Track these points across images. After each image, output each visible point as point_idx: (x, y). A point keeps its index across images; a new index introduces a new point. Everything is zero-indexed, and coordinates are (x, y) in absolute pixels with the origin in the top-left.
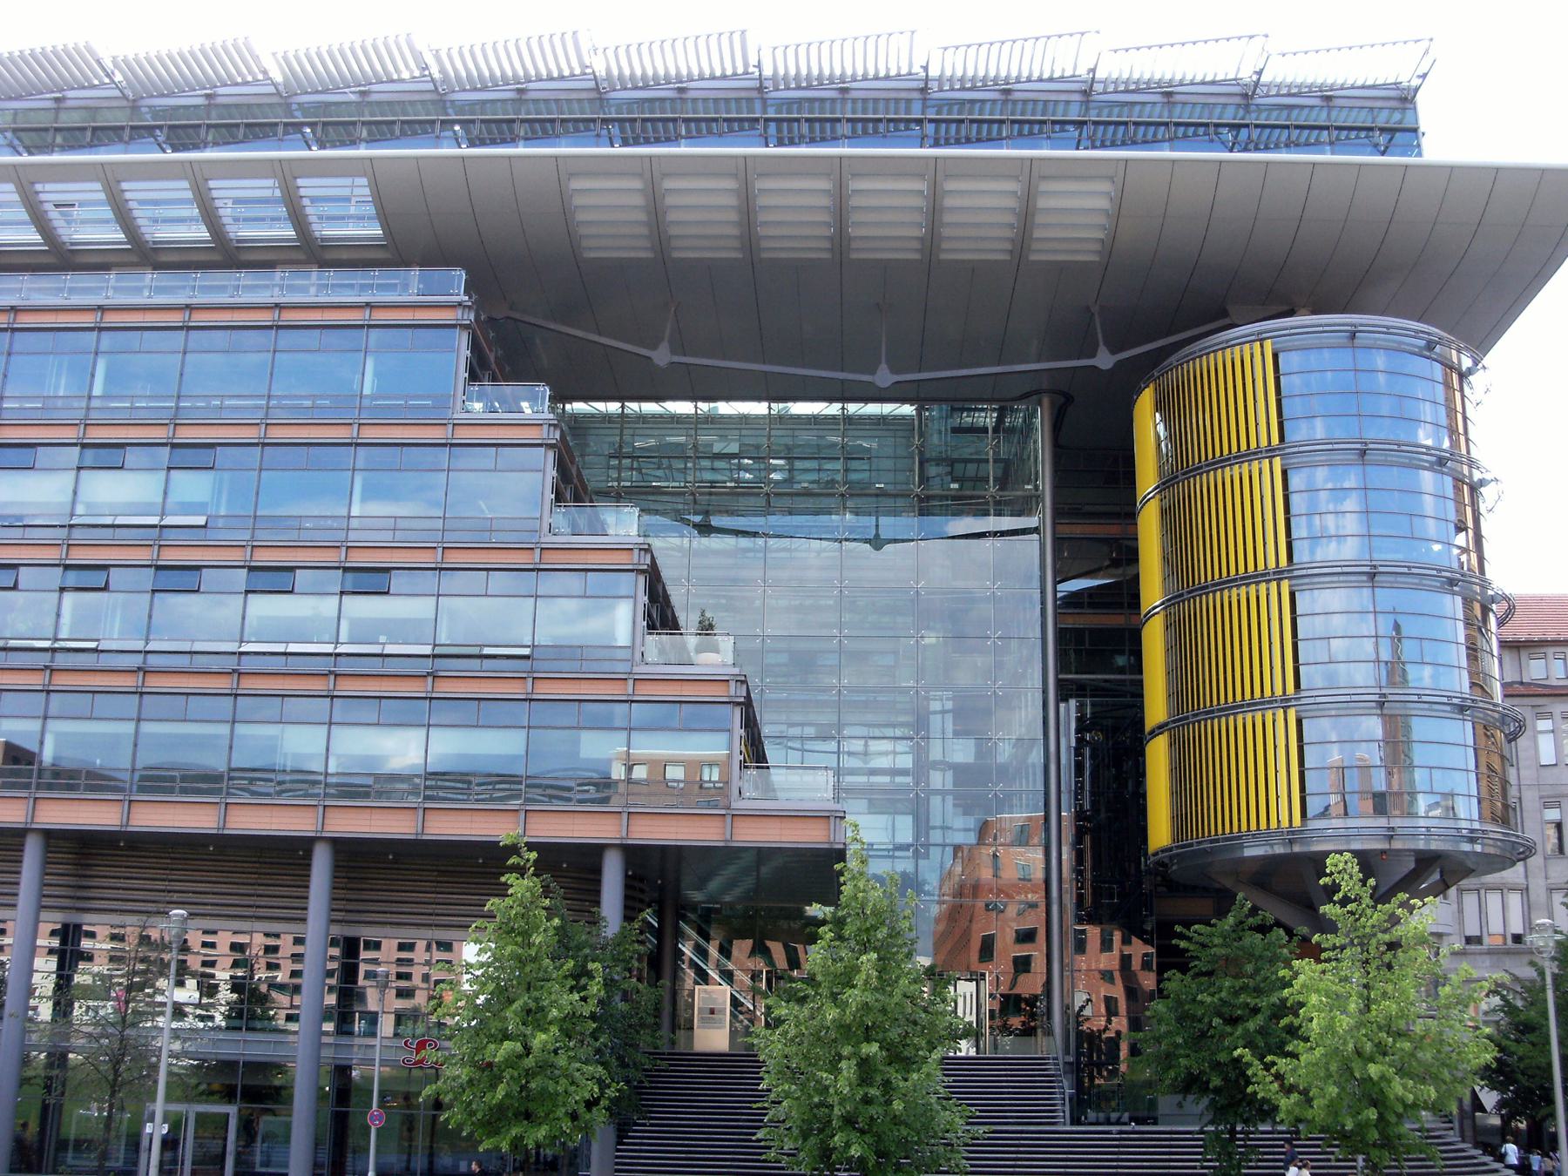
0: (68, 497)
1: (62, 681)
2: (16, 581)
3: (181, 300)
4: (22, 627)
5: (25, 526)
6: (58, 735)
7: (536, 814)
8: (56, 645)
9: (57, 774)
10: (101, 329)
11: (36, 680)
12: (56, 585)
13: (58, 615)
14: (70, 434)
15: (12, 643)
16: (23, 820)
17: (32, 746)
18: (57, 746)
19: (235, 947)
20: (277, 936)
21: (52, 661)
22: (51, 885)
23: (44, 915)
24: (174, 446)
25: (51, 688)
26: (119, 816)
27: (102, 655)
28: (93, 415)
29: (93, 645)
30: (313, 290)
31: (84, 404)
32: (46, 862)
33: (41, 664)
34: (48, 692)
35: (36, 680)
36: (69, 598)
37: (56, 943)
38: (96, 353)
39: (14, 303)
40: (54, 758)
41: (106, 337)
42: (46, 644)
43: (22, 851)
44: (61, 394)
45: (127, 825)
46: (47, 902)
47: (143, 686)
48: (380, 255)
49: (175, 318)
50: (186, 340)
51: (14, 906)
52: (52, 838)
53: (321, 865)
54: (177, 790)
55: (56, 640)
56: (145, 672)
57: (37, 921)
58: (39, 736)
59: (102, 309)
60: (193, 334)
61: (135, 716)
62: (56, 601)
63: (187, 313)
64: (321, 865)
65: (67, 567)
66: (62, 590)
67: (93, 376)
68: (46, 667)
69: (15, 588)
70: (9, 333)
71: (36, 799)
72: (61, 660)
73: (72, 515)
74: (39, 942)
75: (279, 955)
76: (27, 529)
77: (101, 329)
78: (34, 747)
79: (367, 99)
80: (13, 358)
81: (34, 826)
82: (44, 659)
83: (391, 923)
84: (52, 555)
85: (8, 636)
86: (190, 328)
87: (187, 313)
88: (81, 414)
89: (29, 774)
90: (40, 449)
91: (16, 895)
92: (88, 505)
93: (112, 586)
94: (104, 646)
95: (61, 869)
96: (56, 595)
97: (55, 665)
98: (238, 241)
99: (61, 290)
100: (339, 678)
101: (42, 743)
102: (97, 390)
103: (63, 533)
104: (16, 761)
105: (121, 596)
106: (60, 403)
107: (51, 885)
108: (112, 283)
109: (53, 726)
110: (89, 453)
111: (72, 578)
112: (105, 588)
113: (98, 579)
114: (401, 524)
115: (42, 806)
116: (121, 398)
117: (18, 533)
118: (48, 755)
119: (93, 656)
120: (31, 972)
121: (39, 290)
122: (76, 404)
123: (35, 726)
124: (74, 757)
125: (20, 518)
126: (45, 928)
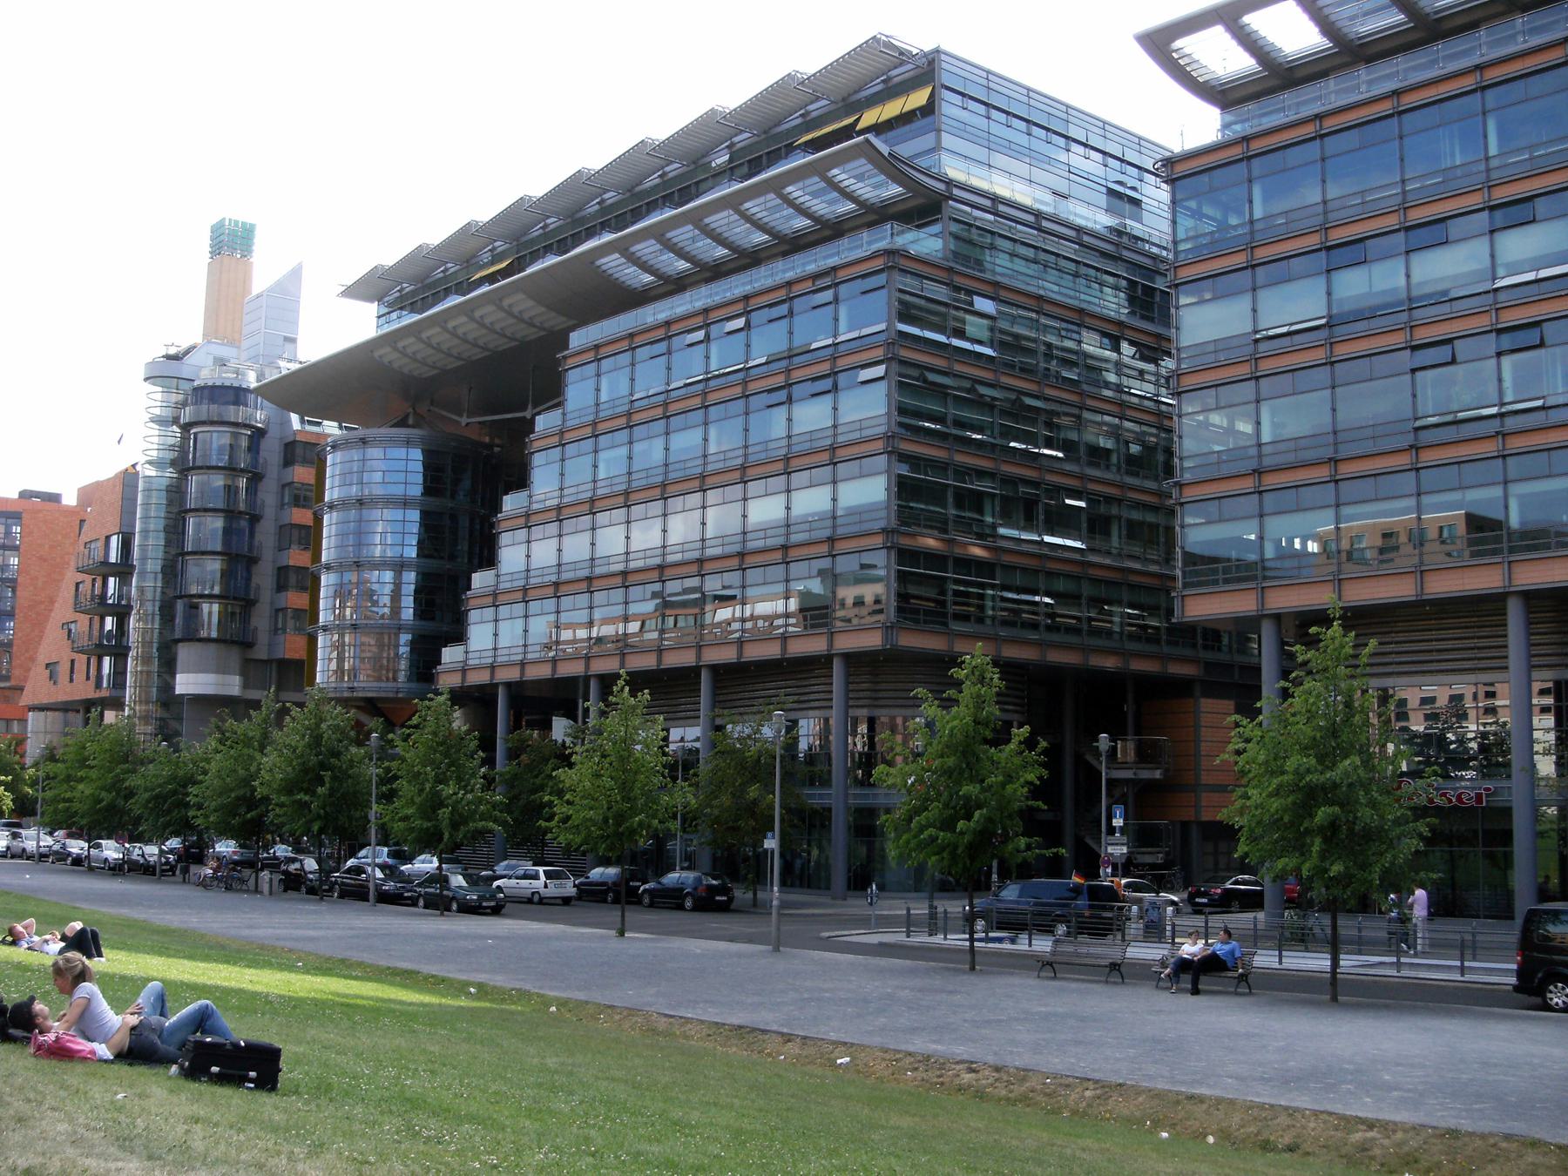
0: (1487, 262)
1: (1516, 443)
2: (1542, 339)
3: (1475, 60)
4: (1467, 399)
5: (1451, 300)
6: (1520, 497)
7: (1520, 564)
8: (1503, 410)
9: (1525, 534)
10: (1484, 88)
11: (1490, 448)
12: (1492, 350)
13: (1500, 380)
14: (1392, 221)
15: (1461, 415)
16: (1500, 584)
17: (1497, 514)
18: (1522, 512)
19: (1424, 701)
20: (1492, 684)
21: (1502, 426)
22: (1539, 645)
23: (1535, 674)
24: (1408, 229)
25: (1419, 465)
26: (1501, 578)
27: (1550, 411)
28: (1494, 175)
29: (1539, 403)
30: (1363, 88)
31: (1482, 167)
32: (1529, 623)
33: (1492, 431)
34: (1504, 457)
35: (1490, 448)
36: (1507, 362)
37: (1549, 701)
38: (1484, 113)
39: (1316, 111)
40: (1522, 523)
41: (1490, 95)
42: (1494, 410)
43: (1505, 614)
44: (1458, 163)
45: (1422, 594)
46: (1535, 661)
47: (1504, 449)
48: (1337, 61)
49: (1308, 130)
50: (1322, 148)
51: (1506, 668)
52: (1531, 597)
53: (1515, 614)
54: (1553, 545)
55: (1502, 404)
56: (1417, 449)
57: (1530, 682)
58: (1502, 502)
59: (1479, 68)
60: (1406, 117)
61: (1414, 491)
62: (1495, 367)
63: (1478, 74)
64: (1515, 614)
65: (1500, 331)
66: (1499, 354)
67: (1485, 136)
68: (1330, 459)
69: (1453, 361)
70: (1318, 141)
71: (1510, 562)
72: (1511, 423)
73: (1494, 279)
74: (1535, 701)
75: (1437, 705)
76: (1454, 303)
77: (1484, 88)
78: (1499, 516)
79: (890, 84)
80: (1406, 141)
81: (1512, 589)
82: (1494, 425)
83: (1479, 669)
84: (1483, 322)
85: (1455, 408)
86: (1322, 136)
87: (1478, 74)
88: (1482, 177)
89: (1498, 540)
90: (1369, 243)
91: (1506, 657)
92: (1507, 265)
93: (1548, 341)
94: (1551, 402)
95: (1542, 628)
96: (1493, 361)
97: (1506, 429)
98: (1436, 13)
99: (1435, 61)
100: (1507, 437)
101: (1506, 507)
102: (1493, 150)
103: (1490, 298)
104: (1480, 529)
105: (1558, 350)
106: (1459, 172)
107: (1539, 645)
108: (1483, 39)
109: (1516, 489)
110: (1498, 214)
111: (1507, 341)
112: (1542, 345)
113: (1533, 336)
114: (865, 424)
115: (1517, 569)
116: (1519, 151)
117: (1446, 308)
118: (1514, 521)
119: (1542, 414)
120: (1531, 729)
121: (1415, 69)
122: (1475, 169)
123: (1497, 492)
124: (1538, 518)
125: (1445, 293)
126: (1536, 686)
